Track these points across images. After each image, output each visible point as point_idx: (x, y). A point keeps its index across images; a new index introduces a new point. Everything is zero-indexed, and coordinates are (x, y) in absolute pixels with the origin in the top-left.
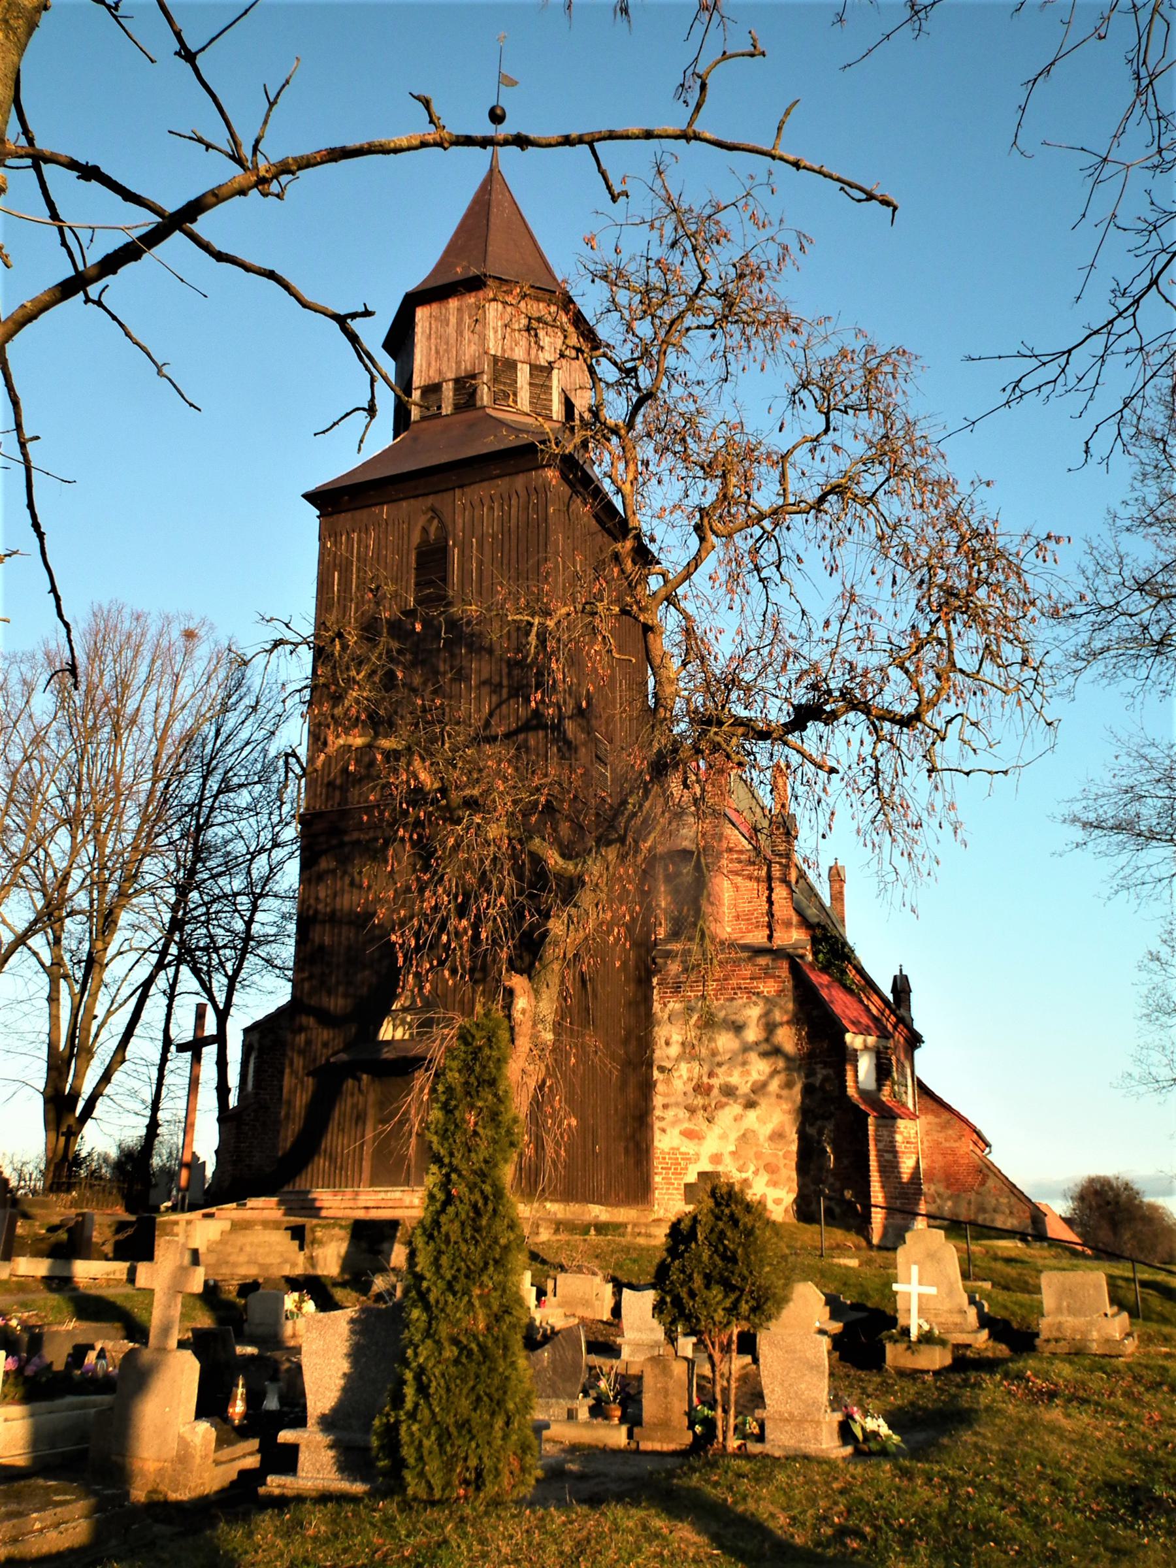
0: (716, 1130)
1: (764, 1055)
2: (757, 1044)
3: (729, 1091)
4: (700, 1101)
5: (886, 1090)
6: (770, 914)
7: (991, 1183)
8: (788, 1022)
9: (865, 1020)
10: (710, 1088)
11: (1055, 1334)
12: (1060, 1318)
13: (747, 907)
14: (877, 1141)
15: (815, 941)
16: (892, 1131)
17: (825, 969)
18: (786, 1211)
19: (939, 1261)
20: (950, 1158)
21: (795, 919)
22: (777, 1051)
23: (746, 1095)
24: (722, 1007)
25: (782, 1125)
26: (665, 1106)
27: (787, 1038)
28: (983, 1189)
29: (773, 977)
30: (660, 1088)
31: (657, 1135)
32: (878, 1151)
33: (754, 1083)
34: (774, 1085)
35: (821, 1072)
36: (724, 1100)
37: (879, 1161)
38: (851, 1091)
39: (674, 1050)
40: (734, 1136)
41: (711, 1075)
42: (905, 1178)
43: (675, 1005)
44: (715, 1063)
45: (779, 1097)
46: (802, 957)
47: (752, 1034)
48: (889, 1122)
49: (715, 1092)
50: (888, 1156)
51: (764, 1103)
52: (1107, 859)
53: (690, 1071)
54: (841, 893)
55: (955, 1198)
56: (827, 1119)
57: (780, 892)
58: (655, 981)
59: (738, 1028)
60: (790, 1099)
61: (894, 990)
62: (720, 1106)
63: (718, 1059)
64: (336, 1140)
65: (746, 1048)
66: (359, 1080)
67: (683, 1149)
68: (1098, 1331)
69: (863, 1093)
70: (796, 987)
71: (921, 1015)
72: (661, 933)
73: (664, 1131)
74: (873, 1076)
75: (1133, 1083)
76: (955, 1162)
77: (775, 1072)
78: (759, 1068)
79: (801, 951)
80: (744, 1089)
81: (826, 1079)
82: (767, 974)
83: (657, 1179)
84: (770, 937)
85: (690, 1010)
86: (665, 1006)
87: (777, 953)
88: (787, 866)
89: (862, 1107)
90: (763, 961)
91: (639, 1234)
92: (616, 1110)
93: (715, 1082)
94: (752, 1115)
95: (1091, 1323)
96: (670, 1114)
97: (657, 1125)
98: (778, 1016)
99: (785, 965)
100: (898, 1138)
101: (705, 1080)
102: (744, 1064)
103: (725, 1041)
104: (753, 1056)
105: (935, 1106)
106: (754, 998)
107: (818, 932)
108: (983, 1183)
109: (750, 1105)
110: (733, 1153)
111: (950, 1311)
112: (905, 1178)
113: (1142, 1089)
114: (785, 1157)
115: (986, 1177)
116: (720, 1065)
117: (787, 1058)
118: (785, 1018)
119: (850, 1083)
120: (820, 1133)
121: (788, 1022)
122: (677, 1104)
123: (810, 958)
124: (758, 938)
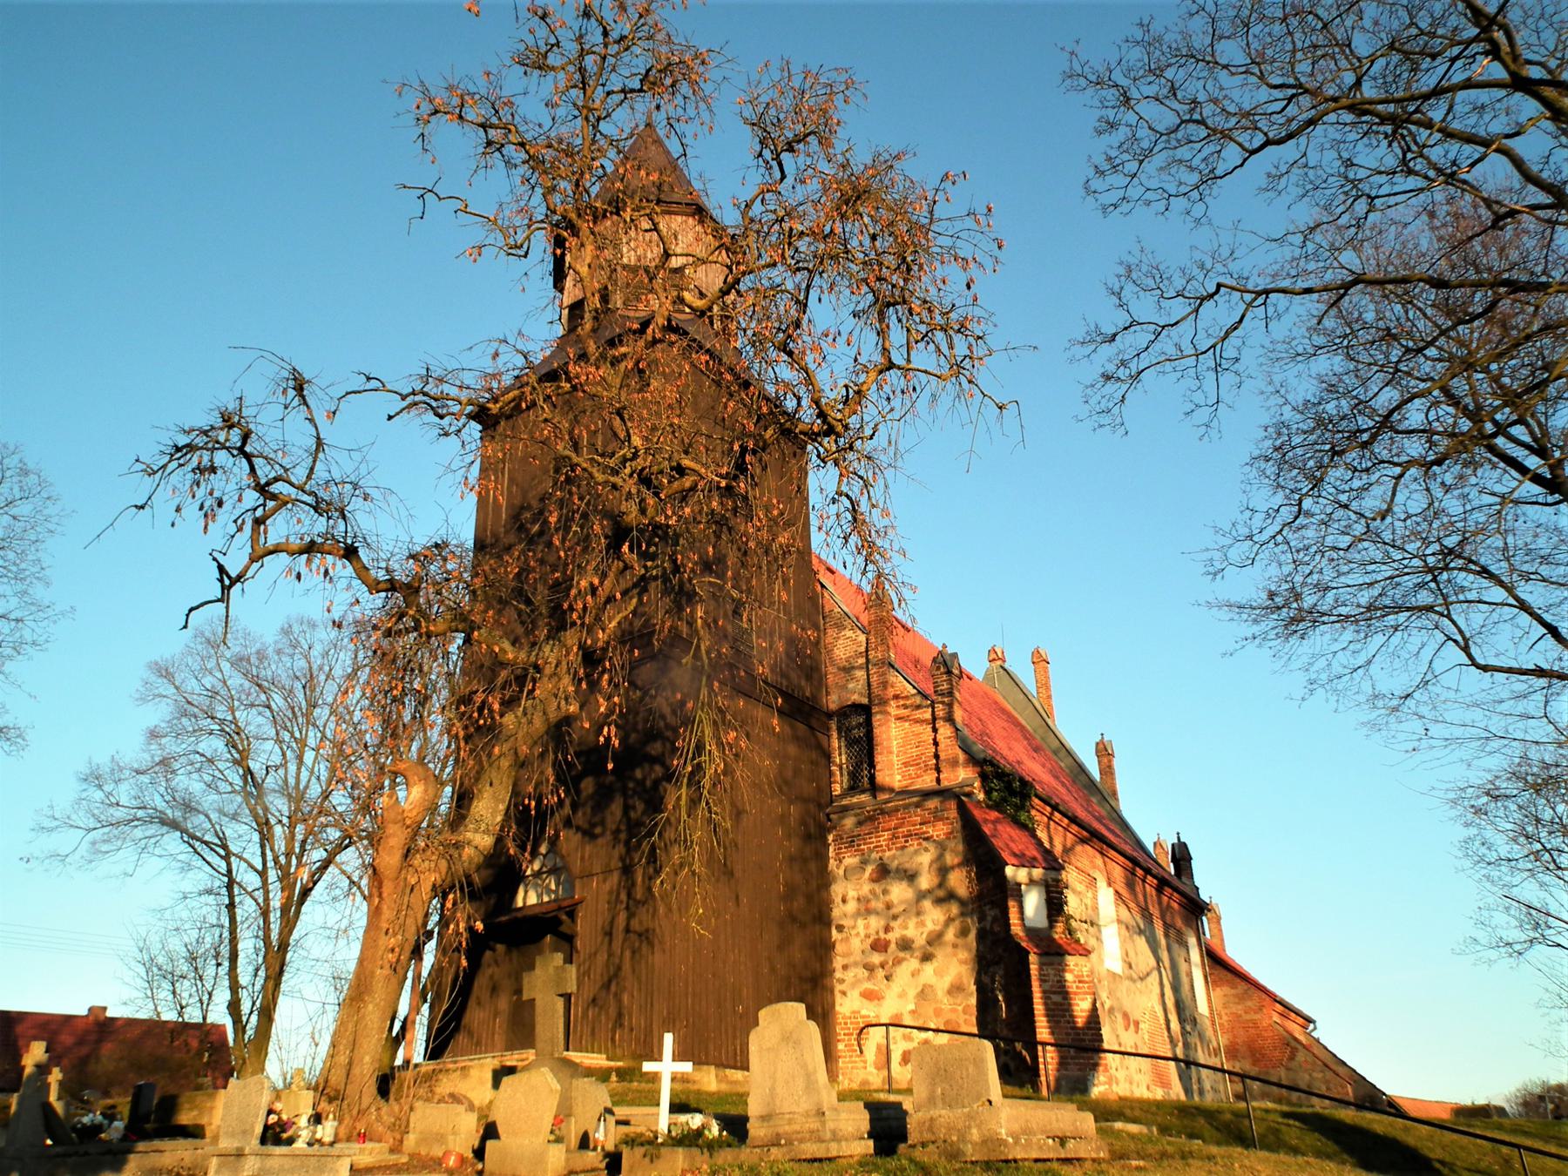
1: (939, 901)
2: (929, 891)
3: (906, 945)
4: (876, 958)
5: (1060, 927)
6: (937, 756)
7: (1301, 1056)
8: (959, 865)
9: (1032, 852)
11: (927, 1136)
12: (934, 1113)
13: (915, 752)
14: (1042, 981)
15: (984, 777)
16: (1061, 969)
17: (997, 806)
19: (797, 1043)
20: (1253, 1031)
21: (961, 756)
22: (951, 896)
23: (922, 947)
24: (894, 857)
25: (960, 976)
26: (845, 967)
27: (960, 881)
28: (1293, 1064)
29: (941, 819)
30: (839, 948)
31: (838, 998)
32: (1044, 992)
33: (930, 933)
34: (950, 935)
35: (991, 913)
36: (902, 955)
37: (1045, 1004)
38: (1016, 929)
39: (851, 906)
40: (912, 993)
41: (887, 929)
42: (1080, 1022)
43: (851, 860)
45: (955, 946)
46: (969, 795)
47: (926, 882)
48: (1056, 959)
49: (893, 946)
51: (941, 954)
53: (867, 927)
54: (1110, 767)
56: (997, 963)
57: (945, 731)
58: (830, 838)
59: (911, 877)
60: (967, 947)
61: (1174, 860)
62: (898, 962)
63: (895, 911)
64: (475, 1016)
65: (921, 896)
66: (493, 950)
67: (864, 1012)
68: (979, 1127)
69: (1032, 933)
70: (964, 827)
71: (1206, 882)
72: (837, 789)
73: (844, 993)
74: (1044, 912)
75: (1478, 948)
76: (1258, 1036)
77: (950, 920)
78: (934, 916)
79: (967, 789)
80: (920, 941)
81: (995, 919)
82: (937, 817)
83: (841, 1046)
84: (938, 781)
85: (864, 862)
86: (841, 861)
87: (942, 793)
88: (950, 705)
89: (1024, 944)
90: (932, 803)
92: (773, 969)
94: (929, 968)
95: (970, 1117)
96: (849, 976)
97: (838, 987)
98: (950, 859)
99: (953, 805)
100: (1069, 977)
101: (882, 935)
102: (918, 914)
103: (899, 892)
104: (927, 904)
105: (1229, 975)
106: (925, 844)
107: (989, 769)
108: (1292, 1058)
109: (927, 958)
110: (913, 1012)
111: (807, 1115)
112: (1080, 1022)
113: (1493, 954)
114: (965, 1012)
115: (1294, 1052)
116: (895, 917)
117: (962, 903)
118: (956, 861)
119: (1014, 919)
120: (993, 982)
121: (959, 865)
122: (856, 964)
123: (981, 796)
124: (927, 781)
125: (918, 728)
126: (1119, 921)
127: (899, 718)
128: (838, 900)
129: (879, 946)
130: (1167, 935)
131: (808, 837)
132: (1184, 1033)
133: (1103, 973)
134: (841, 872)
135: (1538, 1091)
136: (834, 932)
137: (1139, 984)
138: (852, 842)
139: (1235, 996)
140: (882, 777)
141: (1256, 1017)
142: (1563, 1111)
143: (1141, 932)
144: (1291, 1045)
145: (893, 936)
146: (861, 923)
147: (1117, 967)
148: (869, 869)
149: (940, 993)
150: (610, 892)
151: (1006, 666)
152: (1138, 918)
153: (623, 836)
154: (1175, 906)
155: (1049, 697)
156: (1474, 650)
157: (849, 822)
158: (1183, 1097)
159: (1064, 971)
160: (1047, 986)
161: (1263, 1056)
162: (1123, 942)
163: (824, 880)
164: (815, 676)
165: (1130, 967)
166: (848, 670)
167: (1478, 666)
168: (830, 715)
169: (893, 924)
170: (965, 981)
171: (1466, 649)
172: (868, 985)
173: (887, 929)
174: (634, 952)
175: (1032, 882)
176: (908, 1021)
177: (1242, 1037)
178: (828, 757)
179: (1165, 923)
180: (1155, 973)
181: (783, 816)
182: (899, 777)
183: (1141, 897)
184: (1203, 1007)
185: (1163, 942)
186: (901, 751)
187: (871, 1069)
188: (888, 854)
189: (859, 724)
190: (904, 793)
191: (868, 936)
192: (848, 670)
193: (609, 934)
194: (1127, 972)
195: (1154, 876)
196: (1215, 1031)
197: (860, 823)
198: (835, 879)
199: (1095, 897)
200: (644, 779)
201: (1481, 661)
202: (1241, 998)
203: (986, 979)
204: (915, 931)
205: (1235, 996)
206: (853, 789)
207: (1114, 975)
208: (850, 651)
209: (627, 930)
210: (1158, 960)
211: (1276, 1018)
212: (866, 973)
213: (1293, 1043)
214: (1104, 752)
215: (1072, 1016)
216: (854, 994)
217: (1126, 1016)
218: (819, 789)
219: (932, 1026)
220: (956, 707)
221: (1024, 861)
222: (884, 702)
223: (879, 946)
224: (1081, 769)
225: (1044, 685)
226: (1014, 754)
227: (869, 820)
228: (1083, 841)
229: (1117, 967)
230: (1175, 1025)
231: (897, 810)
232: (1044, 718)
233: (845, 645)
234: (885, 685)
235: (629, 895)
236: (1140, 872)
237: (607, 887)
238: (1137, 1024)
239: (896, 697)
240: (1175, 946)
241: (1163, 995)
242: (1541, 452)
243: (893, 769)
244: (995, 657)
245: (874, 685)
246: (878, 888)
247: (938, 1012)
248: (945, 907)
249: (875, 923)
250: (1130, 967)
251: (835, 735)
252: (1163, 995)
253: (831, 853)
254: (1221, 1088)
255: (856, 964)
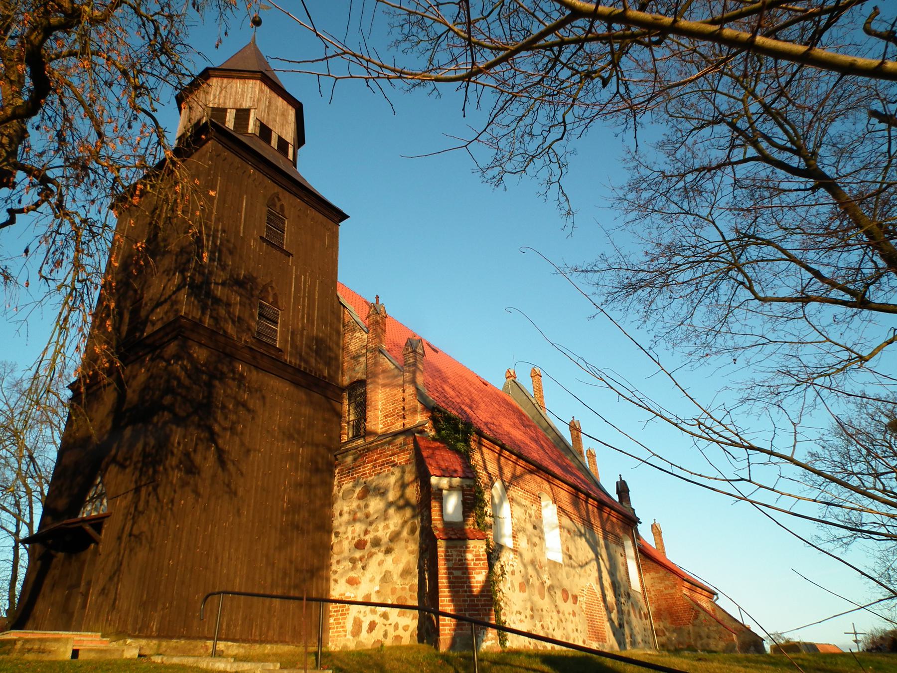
0: (368, 574)
1: (400, 508)
3: (376, 543)
4: (358, 554)
5: (471, 520)
7: (702, 616)
10: (365, 542)
14: (448, 559)
16: (465, 549)
18: (411, 636)
20: (670, 601)
21: (419, 406)
22: (407, 504)
23: (386, 543)
25: (408, 563)
26: (338, 562)
28: (697, 622)
29: (403, 451)
30: (336, 549)
32: (448, 569)
33: (392, 532)
34: (405, 534)
36: (373, 550)
37: (449, 578)
40: (378, 578)
41: (366, 532)
42: (476, 590)
44: (368, 520)
45: (407, 541)
46: (422, 432)
48: (461, 543)
49: (369, 544)
50: (457, 573)
51: (398, 547)
52: (636, 302)
53: (353, 532)
55: (678, 630)
59: (381, 492)
61: (618, 492)
62: (371, 555)
63: (371, 519)
64: (40, 606)
65: (390, 504)
70: (416, 454)
71: (638, 503)
72: (345, 438)
73: (336, 581)
77: (405, 522)
83: (331, 621)
88: (414, 373)
90: (400, 439)
91: (29, 650)
93: (368, 538)
94: (390, 559)
97: (333, 577)
100: (469, 556)
101: (362, 537)
102: (386, 519)
103: (375, 505)
105: (655, 565)
108: (696, 617)
109: (388, 551)
110: (378, 592)
112: (476, 590)
114: (410, 590)
116: (371, 524)
117: (413, 508)
119: (435, 515)
122: (345, 559)
123: (432, 433)
124: (398, 426)
125: (395, 391)
126: (561, 527)
127: (384, 386)
128: (337, 514)
129: (360, 545)
130: (605, 538)
131: (316, 470)
132: (618, 603)
133: (544, 561)
134: (341, 494)
135: (878, 635)
136: (333, 536)
137: (578, 570)
138: (350, 471)
139: (659, 578)
140: (370, 425)
141: (673, 591)
142: (896, 644)
143: (581, 535)
144: (696, 609)
145: (368, 538)
146: (350, 529)
147: (558, 557)
148: (358, 490)
149: (396, 577)
150: (125, 508)
151: (516, 380)
152: (580, 526)
153: (139, 465)
154: (614, 520)
155: (542, 397)
156: (757, 288)
157: (349, 459)
158: (616, 647)
159: (465, 552)
160: (451, 564)
161: (678, 617)
162: (563, 543)
163: (329, 501)
164: (334, 362)
165: (570, 558)
166: (356, 358)
167: (760, 299)
168: (343, 389)
169: (370, 528)
170: (412, 566)
171: (751, 289)
172: (352, 574)
173: (366, 532)
174: (131, 551)
175: (451, 488)
176: (374, 599)
177: (664, 604)
178: (339, 416)
179: (604, 530)
180: (594, 563)
181: (292, 454)
182: (381, 426)
183: (584, 513)
184: (635, 584)
185: (602, 542)
186: (386, 408)
187: (349, 636)
188: (370, 479)
189: (358, 392)
190: (385, 435)
191: (353, 538)
192: (356, 358)
193: (120, 538)
194: (567, 561)
195: (594, 499)
196: (646, 602)
197: (355, 460)
198: (336, 499)
199: (539, 510)
200: (157, 423)
201: (762, 295)
202: (662, 580)
203: (422, 564)
204: (382, 531)
205: (659, 578)
206: (356, 436)
207: (555, 564)
208: (358, 346)
209: (130, 535)
210: (597, 555)
211: (685, 591)
212: (351, 565)
213: (696, 608)
214: (574, 428)
215: (471, 587)
216: (342, 581)
217: (565, 592)
218: (330, 438)
219: (390, 602)
220: (418, 374)
221: (446, 473)
222: (375, 375)
223: (360, 545)
224: (561, 439)
225: (539, 389)
226: (454, 401)
227: (361, 455)
228: (531, 472)
229: (558, 557)
230: (610, 597)
231: (377, 447)
232: (538, 408)
233: (356, 341)
234: (376, 364)
235: (136, 507)
236: (582, 496)
237: (124, 503)
238: (575, 598)
239: (384, 371)
240: (613, 546)
241: (600, 578)
242: (798, 152)
243: (379, 419)
244: (510, 376)
245: (370, 366)
246: (362, 503)
247: (393, 591)
248: (402, 512)
249: (359, 528)
250: (570, 558)
251: (346, 402)
252: (600, 578)
253: (336, 483)
254: (651, 640)
255: (345, 559)
